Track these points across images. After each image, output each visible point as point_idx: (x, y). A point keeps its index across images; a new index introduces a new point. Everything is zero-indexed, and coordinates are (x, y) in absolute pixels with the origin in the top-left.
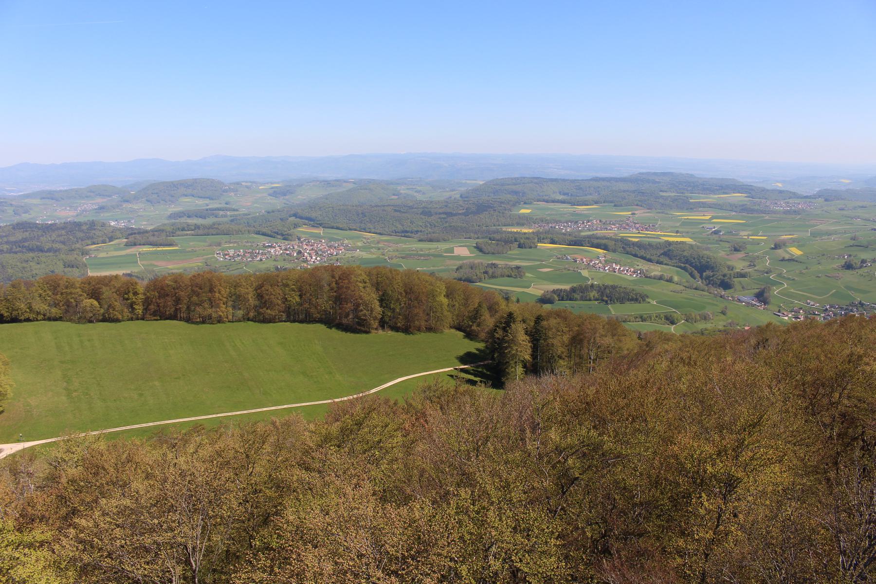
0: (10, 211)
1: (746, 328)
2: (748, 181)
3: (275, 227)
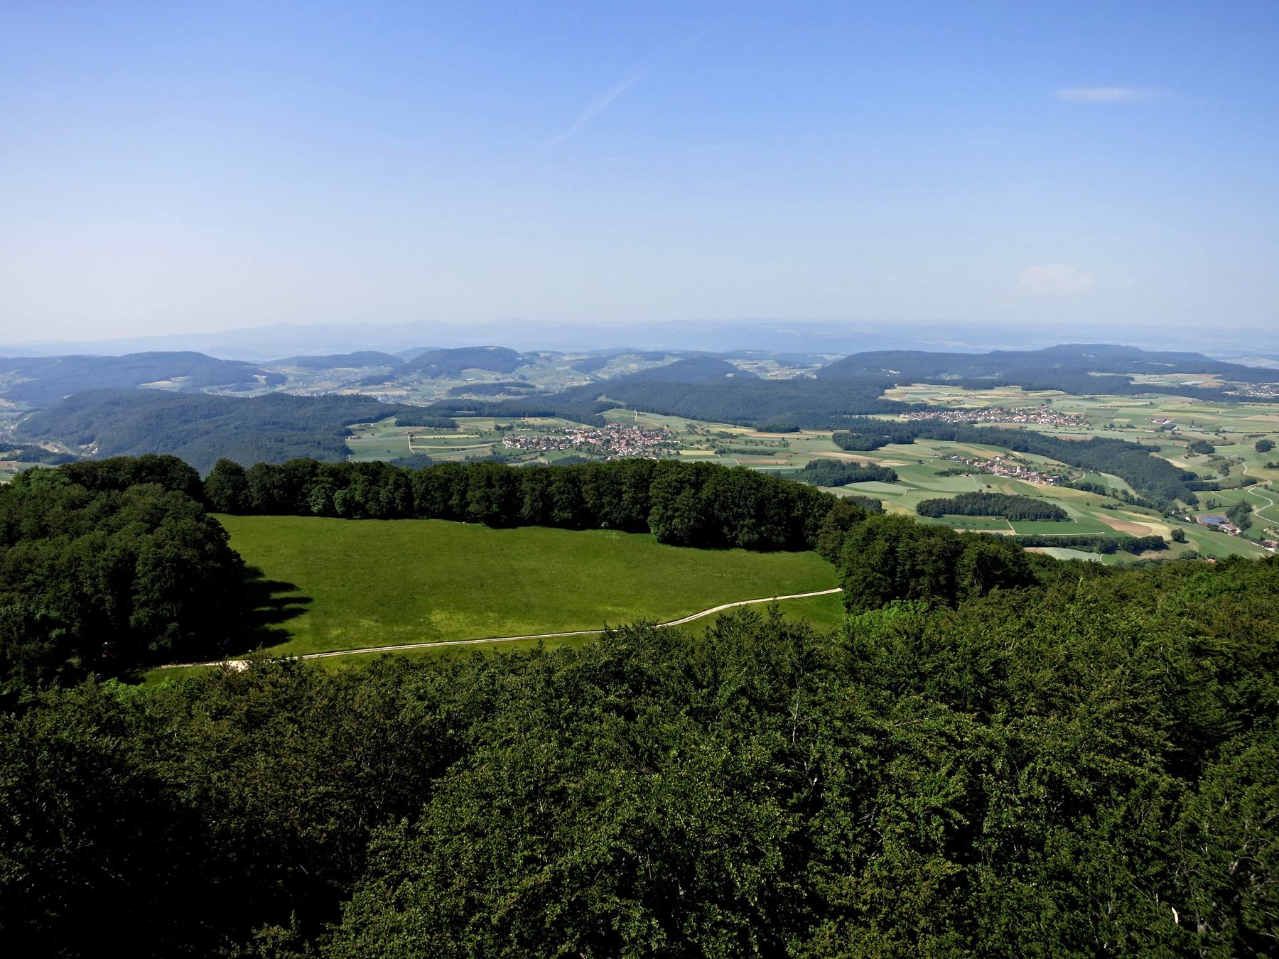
0: (262, 378)
1: (959, 531)
2: (1219, 356)
3: (584, 407)
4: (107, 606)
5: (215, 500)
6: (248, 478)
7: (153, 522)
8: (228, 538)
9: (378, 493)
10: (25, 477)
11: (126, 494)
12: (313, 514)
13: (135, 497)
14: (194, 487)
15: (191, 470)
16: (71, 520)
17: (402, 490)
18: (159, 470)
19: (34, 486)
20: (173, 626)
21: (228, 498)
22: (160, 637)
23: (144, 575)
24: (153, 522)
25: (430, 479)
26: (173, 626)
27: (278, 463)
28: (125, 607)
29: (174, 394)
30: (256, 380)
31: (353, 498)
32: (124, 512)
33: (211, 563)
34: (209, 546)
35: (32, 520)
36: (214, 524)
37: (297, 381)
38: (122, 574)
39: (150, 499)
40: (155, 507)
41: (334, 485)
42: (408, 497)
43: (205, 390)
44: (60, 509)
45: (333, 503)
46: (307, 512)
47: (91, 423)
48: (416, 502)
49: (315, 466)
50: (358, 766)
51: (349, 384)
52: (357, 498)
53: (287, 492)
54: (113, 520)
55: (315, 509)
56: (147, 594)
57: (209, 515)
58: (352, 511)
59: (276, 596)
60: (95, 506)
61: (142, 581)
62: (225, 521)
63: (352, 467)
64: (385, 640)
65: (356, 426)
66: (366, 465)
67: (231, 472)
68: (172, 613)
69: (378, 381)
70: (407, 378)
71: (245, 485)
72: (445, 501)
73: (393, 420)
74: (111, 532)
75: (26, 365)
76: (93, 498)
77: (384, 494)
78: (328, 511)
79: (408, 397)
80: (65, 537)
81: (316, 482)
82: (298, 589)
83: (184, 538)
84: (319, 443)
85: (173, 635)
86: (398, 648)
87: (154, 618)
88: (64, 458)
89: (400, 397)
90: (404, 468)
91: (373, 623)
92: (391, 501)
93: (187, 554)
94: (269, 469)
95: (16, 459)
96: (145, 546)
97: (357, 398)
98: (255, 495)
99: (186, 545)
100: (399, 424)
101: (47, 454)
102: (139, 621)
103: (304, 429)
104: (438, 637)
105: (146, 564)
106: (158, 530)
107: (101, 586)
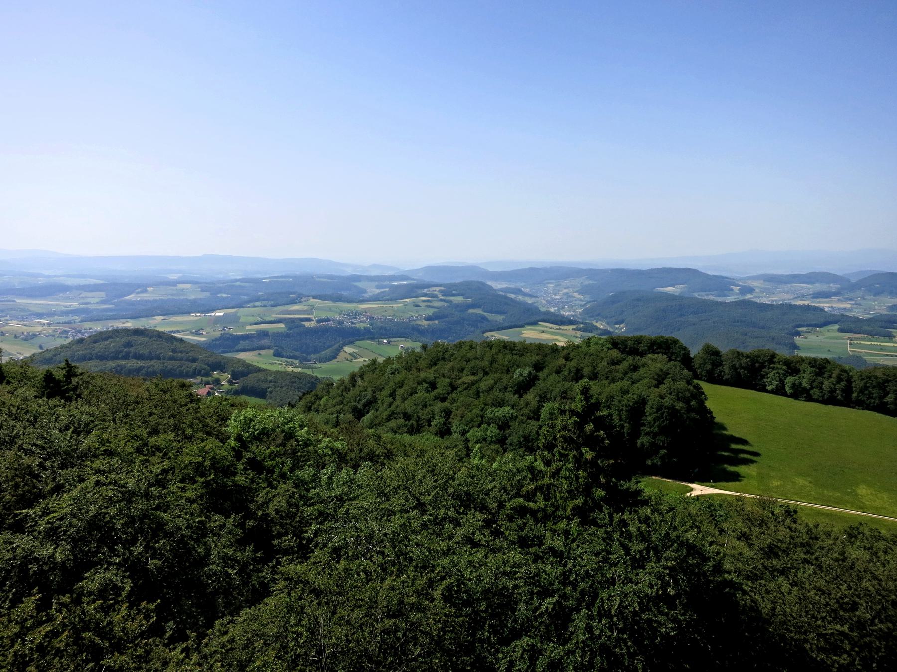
0: (736, 289)
4: (625, 430)
5: (699, 371)
6: (723, 359)
7: (660, 380)
8: (706, 399)
9: (822, 383)
10: (588, 342)
11: (644, 360)
12: (767, 391)
13: (650, 363)
14: (687, 361)
15: (685, 349)
16: (611, 372)
17: (843, 384)
18: (665, 347)
19: (591, 347)
20: (663, 452)
21: (708, 372)
22: (654, 457)
23: (650, 415)
24: (660, 380)
25: (869, 378)
26: (663, 452)
27: (747, 351)
28: (635, 433)
29: (676, 296)
30: (732, 290)
31: (801, 384)
32: (642, 371)
33: (693, 415)
34: (693, 403)
35: (590, 369)
36: (697, 387)
37: (762, 292)
38: (637, 411)
39: (659, 365)
40: (662, 370)
41: (787, 372)
42: (848, 390)
43: (696, 295)
44: (606, 364)
45: (784, 386)
46: (763, 389)
47: (623, 311)
48: (855, 395)
49: (773, 356)
50: (872, 620)
51: (802, 297)
52: (804, 384)
53: (750, 373)
54: (635, 376)
55: (769, 388)
56: (650, 427)
57: (696, 381)
58: (798, 393)
59: (734, 446)
60: (625, 365)
61: (649, 418)
62: (706, 387)
63: (803, 360)
64: (815, 499)
65: (804, 329)
66: (815, 360)
67: (713, 354)
68: (664, 443)
69: (826, 295)
70: (852, 295)
71: (721, 364)
72: (881, 398)
73: (836, 326)
74: (633, 383)
75: (591, 273)
76: (624, 360)
77: (827, 385)
78: (780, 391)
79: (851, 310)
80: (607, 382)
81: (774, 369)
82: (751, 445)
83: (677, 395)
84: (773, 339)
85: (662, 458)
86: (826, 508)
87: (653, 444)
88: (606, 332)
89: (845, 309)
90: (847, 367)
91: (807, 483)
92: (832, 391)
93: (679, 405)
94: (739, 355)
95: (580, 329)
96: (653, 396)
97: (807, 308)
98: (727, 372)
99: (678, 399)
100: (841, 330)
101: (597, 328)
102: (643, 444)
103: (763, 328)
104: (862, 508)
105: (652, 408)
106: (662, 387)
107: (623, 417)
